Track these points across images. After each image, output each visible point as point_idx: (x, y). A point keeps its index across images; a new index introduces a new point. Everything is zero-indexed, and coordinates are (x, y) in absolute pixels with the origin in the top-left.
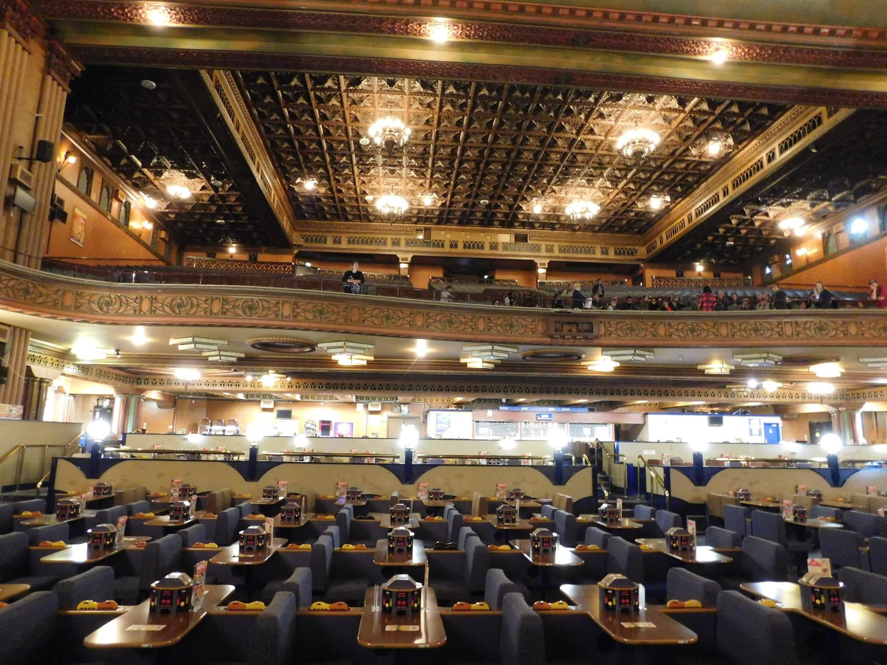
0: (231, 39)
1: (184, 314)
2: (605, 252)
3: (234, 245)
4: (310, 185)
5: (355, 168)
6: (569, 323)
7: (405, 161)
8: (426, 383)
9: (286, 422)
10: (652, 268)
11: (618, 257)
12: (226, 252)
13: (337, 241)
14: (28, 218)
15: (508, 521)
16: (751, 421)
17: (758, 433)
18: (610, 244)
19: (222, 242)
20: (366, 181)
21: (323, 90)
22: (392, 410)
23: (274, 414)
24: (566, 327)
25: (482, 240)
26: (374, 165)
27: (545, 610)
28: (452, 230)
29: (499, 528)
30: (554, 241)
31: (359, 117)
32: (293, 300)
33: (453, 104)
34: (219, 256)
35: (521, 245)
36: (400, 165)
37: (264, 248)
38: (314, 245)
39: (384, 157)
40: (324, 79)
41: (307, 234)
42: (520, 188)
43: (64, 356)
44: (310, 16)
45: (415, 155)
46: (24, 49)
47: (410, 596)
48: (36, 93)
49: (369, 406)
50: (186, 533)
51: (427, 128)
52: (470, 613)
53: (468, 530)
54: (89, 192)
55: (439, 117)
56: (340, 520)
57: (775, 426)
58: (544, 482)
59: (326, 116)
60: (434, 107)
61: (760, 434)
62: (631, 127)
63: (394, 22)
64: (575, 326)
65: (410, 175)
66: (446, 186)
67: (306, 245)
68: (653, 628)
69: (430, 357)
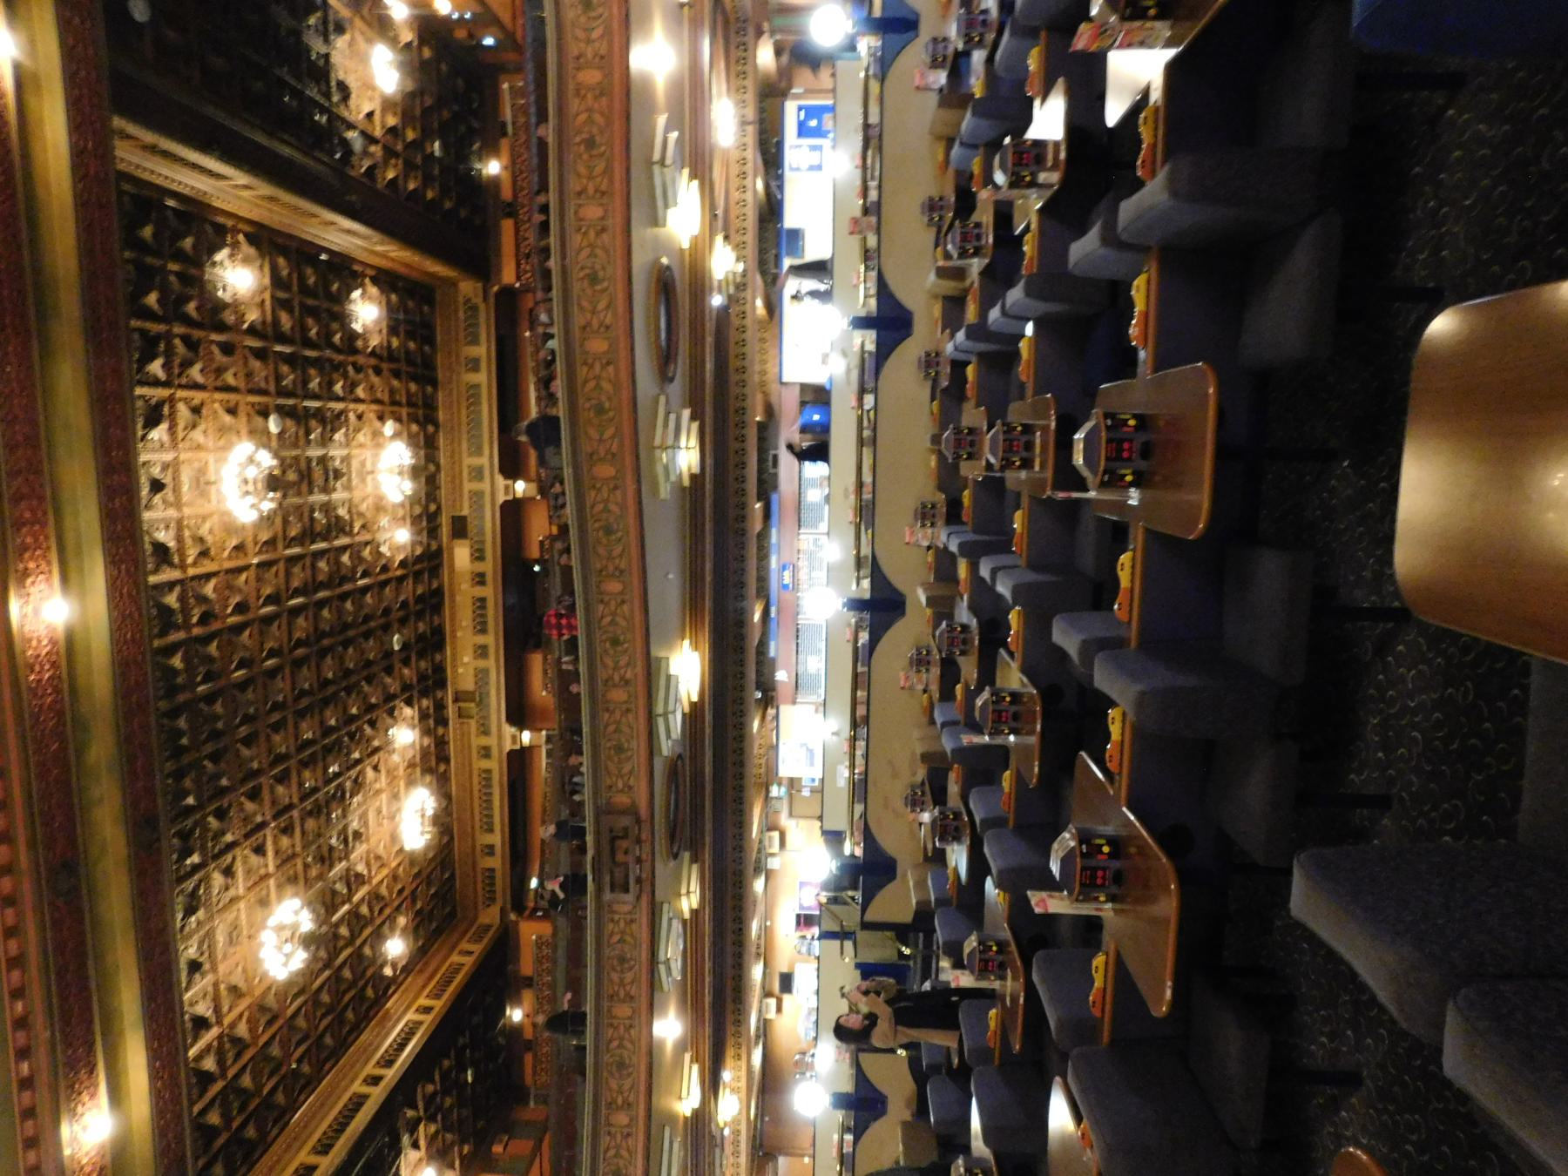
1: (629, 636)
2: (474, 365)
3: (508, 1012)
4: (396, 947)
5: (338, 543)
7: (315, 452)
9: (797, 983)
10: (499, 271)
11: (483, 336)
13: (490, 851)
15: (978, 237)
16: (794, 166)
17: (818, 153)
18: (458, 356)
20: (379, 864)
21: (185, 610)
22: (777, 812)
23: (786, 998)
24: (620, 857)
25: (469, 602)
26: (327, 508)
28: (454, 655)
29: (990, 254)
30: (461, 465)
31: (234, 542)
33: (187, 364)
34: (507, 193)
35: (472, 528)
36: (323, 460)
39: (311, 492)
40: (166, 611)
41: (480, 899)
42: (371, 708)
45: (301, 432)
49: (771, 851)
50: (982, 821)
51: (242, 409)
53: (994, 314)
55: (218, 389)
56: (973, 552)
57: (802, 113)
59: (237, 604)
60: (196, 402)
61: (818, 148)
62: (218, 491)
64: (618, 843)
65: (343, 439)
66: (358, 369)
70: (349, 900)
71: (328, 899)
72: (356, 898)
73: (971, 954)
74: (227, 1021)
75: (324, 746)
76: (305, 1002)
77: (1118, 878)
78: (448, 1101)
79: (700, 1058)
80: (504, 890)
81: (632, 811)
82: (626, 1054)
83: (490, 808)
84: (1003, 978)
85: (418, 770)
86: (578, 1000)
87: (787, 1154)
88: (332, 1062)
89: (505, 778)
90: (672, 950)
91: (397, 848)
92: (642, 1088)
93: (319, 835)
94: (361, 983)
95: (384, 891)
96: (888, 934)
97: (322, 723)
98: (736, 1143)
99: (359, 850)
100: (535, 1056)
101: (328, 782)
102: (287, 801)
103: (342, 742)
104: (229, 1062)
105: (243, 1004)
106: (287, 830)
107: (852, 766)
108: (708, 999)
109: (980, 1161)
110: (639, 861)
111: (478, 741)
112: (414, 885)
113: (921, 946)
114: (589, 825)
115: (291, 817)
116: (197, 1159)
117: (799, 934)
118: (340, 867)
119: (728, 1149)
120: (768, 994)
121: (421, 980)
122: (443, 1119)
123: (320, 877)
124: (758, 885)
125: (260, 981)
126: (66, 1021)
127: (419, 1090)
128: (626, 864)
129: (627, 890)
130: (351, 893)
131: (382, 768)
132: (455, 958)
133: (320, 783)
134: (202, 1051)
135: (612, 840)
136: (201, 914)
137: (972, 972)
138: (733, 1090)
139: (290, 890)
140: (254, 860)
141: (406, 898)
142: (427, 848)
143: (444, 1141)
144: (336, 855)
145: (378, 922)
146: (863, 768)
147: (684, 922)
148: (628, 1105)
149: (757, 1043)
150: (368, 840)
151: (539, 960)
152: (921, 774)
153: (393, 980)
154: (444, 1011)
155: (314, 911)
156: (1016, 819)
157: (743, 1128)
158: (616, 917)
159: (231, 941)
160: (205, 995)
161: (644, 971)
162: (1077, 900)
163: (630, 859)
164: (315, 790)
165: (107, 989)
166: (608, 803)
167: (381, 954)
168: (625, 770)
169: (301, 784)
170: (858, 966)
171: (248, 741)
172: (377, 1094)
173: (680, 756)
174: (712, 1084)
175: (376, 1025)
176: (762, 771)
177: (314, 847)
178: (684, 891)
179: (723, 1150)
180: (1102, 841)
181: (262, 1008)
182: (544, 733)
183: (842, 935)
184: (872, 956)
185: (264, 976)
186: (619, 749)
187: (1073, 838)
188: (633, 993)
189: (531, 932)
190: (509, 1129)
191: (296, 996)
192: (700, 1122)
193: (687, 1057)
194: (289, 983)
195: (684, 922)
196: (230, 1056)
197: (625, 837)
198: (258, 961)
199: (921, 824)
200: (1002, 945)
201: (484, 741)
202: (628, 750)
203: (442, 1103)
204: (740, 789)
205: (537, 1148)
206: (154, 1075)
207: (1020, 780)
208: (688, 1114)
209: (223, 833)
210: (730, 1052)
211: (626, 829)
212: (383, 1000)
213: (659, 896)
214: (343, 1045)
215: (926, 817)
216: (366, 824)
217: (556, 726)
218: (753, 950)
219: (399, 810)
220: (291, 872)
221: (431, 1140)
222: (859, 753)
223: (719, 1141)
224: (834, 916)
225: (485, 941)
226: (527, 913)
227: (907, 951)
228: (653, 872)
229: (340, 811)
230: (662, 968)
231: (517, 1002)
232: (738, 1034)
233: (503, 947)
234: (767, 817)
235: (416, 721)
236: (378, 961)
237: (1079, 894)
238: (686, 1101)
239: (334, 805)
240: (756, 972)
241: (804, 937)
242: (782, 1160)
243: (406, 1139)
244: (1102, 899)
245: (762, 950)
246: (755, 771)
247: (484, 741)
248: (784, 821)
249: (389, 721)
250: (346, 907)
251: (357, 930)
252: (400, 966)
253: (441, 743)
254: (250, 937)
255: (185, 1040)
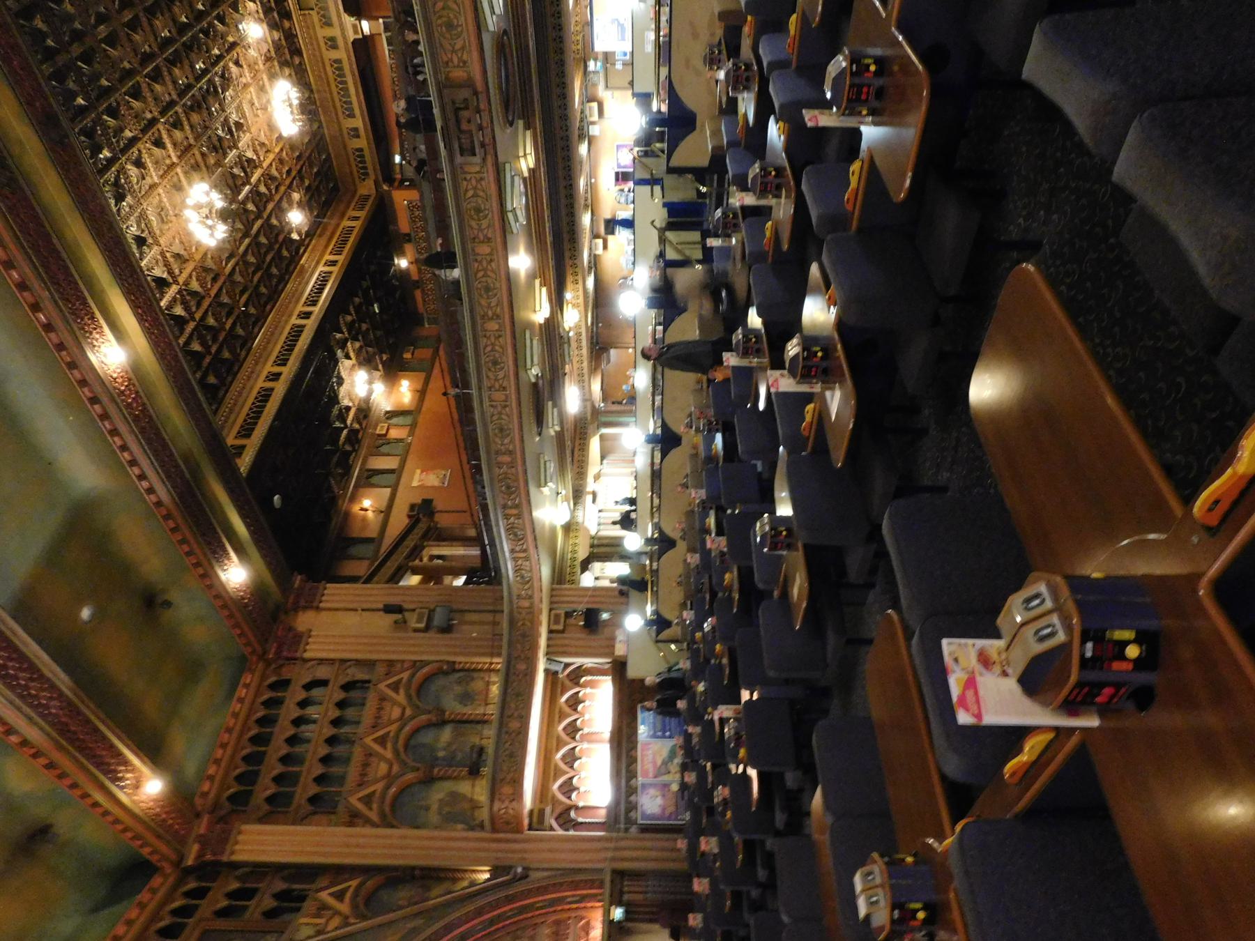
0: (220, 504)
1: (516, 484)
3: (396, 261)
4: (296, 218)
6: (458, 121)
8: (557, 118)
11: (367, 208)
12: (408, 270)
13: (355, 133)
14: (455, 607)
19: (397, 280)
20: (264, 150)
22: (595, 85)
23: (610, 238)
24: (464, 126)
27: (857, 194)
32: (493, 456)
34: (415, 276)
37: (391, 227)
38: (369, 165)
43: (568, 528)
44: (168, 477)
46: (310, 637)
47: (857, 81)
48: (340, 614)
50: (769, 64)
52: (860, 192)
54: (392, 471)
58: (675, 454)
63: (129, 406)
67: (372, 177)
68: (831, 418)
69: (530, 249)
70: (248, 183)
71: (230, 182)
72: (253, 180)
73: (755, 177)
74: (181, 280)
75: (184, 44)
76: (237, 264)
77: (880, 93)
78: (364, 326)
79: (548, 283)
80: (374, 164)
81: (469, 84)
82: (489, 281)
83: (346, 90)
84: (778, 196)
85: (276, 63)
86: (447, 242)
87: (615, 348)
88: (271, 303)
89: (355, 66)
90: (517, 201)
91: (276, 135)
92: (506, 304)
93: (206, 128)
94: (277, 246)
95: (274, 172)
96: (690, 176)
97: (174, 20)
98: (579, 341)
99: (244, 140)
100: (423, 291)
101: (198, 78)
102: (168, 98)
103: (198, 39)
104: (194, 309)
105: (190, 267)
106: (177, 125)
107: (658, 29)
108: (549, 239)
109: (755, 332)
110: (481, 128)
111: (323, 33)
112: (298, 167)
113: (715, 184)
114: (433, 98)
115: (176, 112)
116: (194, 373)
117: (618, 188)
118: (232, 155)
119: (574, 344)
120: (596, 236)
121: (323, 241)
122: (363, 337)
123: (218, 164)
124: (583, 149)
125: (197, 249)
126: (56, 283)
127: (341, 320)
128: (470, 132)
129: (474, 154)
130: (248, 177)
131: (242, 62)
132: (346, 223)
133: (192, 81)
134: (170, 302)
135: (455, 111)
136: (129, 199)
137: (755, 194)
138: (574, 305)
139: (195, 176)
140: (156, 151)
141: (294, 178)
142: (302, 133)
143: (367, 352)
144: (226, 144)
145: (277, 198)
146: (668, 31)
147: (524, 179)
148: (497, 317)
149: (589, 273)
150: (249, 130)
151: (413, 220)
152: (719, 32)
153: (301, 242)
154: (347, 263)
155: (221, 192)
156: (798, 61)
157: (583, 330)
158: (468, 177)
159: (162, 220)
160: (157, 262)
161: (496, 218)
162: (843, 115)
163: (473, 127)
164: (189, 87)
165: (79, 261)
166: (447, 78)
167: (288, 223)
168: (457, 47)
169: (175, 82)
170: (665, 205)
171: (112, 40)
172: (311, 325)
173: (505, 32)
174: (558, 302)
175: (298, 276)
176: (579, 47)
177: (205, 138)
178: (521, 154)
179: (569, 345)
180: (870, 61)
181: (206, 270)
182: (381, 21)
183: (652, 181)
184: (675, 197)
185: (199, 245)
186: (450, 26)
187: (845, 59)
188: (490, 235)
189: (402, 199)
190: (414, 343)
191: (229, 259)
192: (551, 329)
193: (537, 282)
194: (219, 249)
195: (524, 179)
196: (193, 303)
197: (467, 108)
198: (189, 234)
199: (717, 81)
200: (780, 171)
201: (329, 32)
202: (458, 26)
203: (360, 328)
204: (561, 63)
205: (437, 350)
206: (141, 319)
207: (805, 21)
208: (542, 321)
209: (122, 130)
210: (570, 279)
211: (466, 100)
212: (297, 258)
213: (501, 159)
214: (275, 294)
215: (721, 75)
216: (244, 116)
217: (391, 14)
218: (582, 202)
219: (268, 101)
220: (192, 161)
221: (358, 352)
222: (664, 19)
223: (566, 340)
224: (645, 166)
225: (367, 208)
226: (396, 184)
227: (704, 189)
228: (494, 138)
229: (217, 106)
230: (510, 215)
231: (402, 254)
232: (575, 266)
233: (382, 213)
234: (586, 90)
235: (262, 16)
236: (284, 229)
237: (846, 109)
238: (540, 312)
239: (211, 99)
240: (586, 219)
241: (622, 190)
242: (613, 352)
243: (339, 353)
244: (864, 112)
245: (590, 201)
246: (574, 48)
247: (329, 32)
248: (602, 92)
249: (236, 16)
250: (247, 188)
251: (261, 205)
252: (303, 232)
253: (290, 36)
254: (176, 216)
255: (154, 295)
